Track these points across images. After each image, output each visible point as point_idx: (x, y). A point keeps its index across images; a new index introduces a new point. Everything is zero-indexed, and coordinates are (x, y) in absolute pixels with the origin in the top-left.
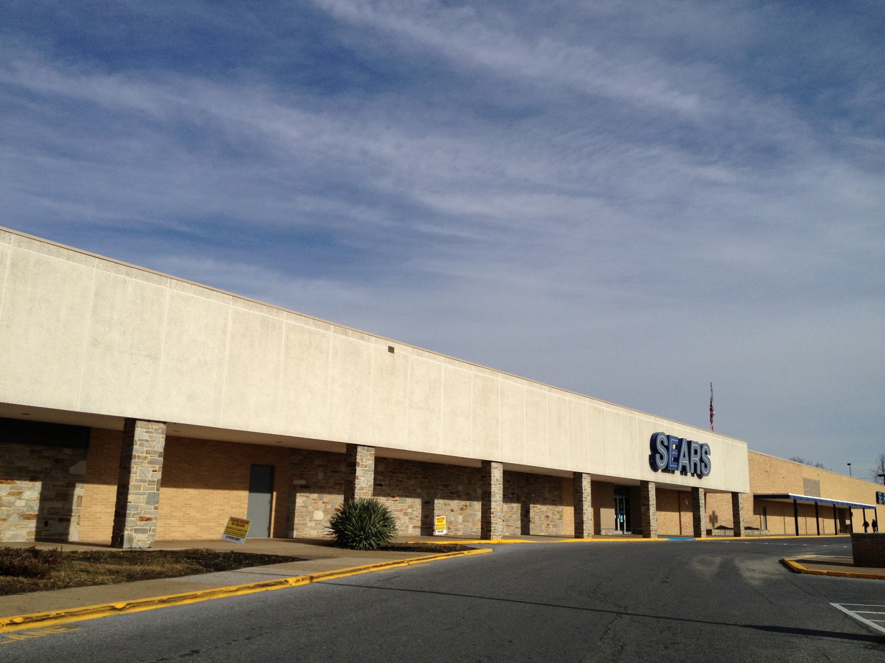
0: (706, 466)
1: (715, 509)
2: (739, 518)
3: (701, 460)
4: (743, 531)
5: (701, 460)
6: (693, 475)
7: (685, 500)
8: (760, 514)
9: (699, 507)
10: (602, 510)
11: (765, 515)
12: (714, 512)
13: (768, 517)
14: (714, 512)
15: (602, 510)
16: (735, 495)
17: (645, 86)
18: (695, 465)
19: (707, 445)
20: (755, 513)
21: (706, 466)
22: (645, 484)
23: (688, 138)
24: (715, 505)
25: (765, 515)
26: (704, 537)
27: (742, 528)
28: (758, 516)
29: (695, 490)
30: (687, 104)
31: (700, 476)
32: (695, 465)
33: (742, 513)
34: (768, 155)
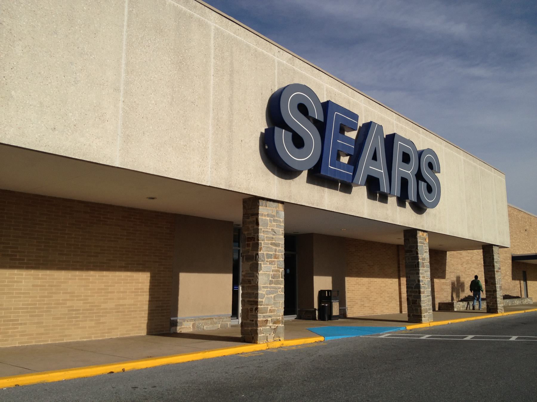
0: (429, 189)
1: (459, 273)
2: (494, 284)
3: (419, 176)
4: (501, 303)
5: (419, 176)
6: (401, 202)
7: (396, 254)
8: (520, 280)
9: (417, 265)
10: (435, 280)
11: (525, 280)
12: (458, 278)
13: (529, 283)
14: (458, 278)
15: (435, 280)
16: (488, 250)
17: (434, 22)
18: (404, 182)
19: (430, 151)
20: (514, 278)
21: (429, 189)
22: (251, 203)
23: (461, 51)
24: (460, 267)
25: (525, 280)
26: (428, 321)
27: (499, 299)
28: (517, 282)
29: (411, 234)
30: (460, 30)
31: (419, 207)
32: (404, 182)
33: (498, 276)
34: (511, 58)
